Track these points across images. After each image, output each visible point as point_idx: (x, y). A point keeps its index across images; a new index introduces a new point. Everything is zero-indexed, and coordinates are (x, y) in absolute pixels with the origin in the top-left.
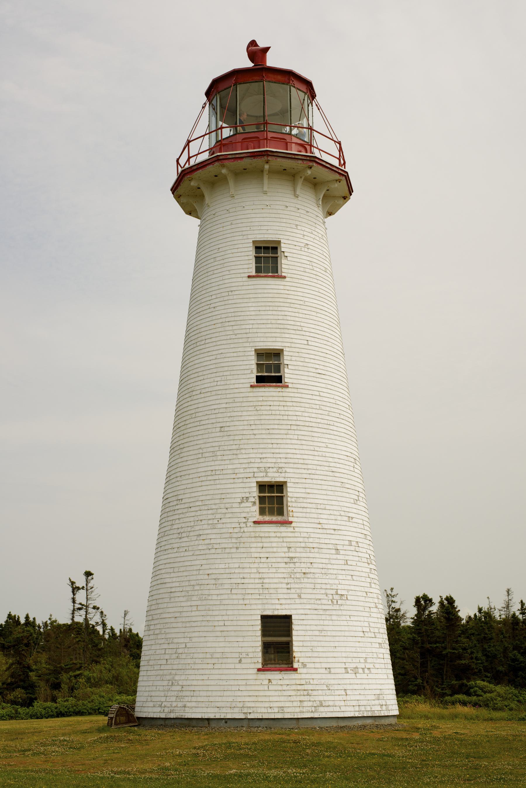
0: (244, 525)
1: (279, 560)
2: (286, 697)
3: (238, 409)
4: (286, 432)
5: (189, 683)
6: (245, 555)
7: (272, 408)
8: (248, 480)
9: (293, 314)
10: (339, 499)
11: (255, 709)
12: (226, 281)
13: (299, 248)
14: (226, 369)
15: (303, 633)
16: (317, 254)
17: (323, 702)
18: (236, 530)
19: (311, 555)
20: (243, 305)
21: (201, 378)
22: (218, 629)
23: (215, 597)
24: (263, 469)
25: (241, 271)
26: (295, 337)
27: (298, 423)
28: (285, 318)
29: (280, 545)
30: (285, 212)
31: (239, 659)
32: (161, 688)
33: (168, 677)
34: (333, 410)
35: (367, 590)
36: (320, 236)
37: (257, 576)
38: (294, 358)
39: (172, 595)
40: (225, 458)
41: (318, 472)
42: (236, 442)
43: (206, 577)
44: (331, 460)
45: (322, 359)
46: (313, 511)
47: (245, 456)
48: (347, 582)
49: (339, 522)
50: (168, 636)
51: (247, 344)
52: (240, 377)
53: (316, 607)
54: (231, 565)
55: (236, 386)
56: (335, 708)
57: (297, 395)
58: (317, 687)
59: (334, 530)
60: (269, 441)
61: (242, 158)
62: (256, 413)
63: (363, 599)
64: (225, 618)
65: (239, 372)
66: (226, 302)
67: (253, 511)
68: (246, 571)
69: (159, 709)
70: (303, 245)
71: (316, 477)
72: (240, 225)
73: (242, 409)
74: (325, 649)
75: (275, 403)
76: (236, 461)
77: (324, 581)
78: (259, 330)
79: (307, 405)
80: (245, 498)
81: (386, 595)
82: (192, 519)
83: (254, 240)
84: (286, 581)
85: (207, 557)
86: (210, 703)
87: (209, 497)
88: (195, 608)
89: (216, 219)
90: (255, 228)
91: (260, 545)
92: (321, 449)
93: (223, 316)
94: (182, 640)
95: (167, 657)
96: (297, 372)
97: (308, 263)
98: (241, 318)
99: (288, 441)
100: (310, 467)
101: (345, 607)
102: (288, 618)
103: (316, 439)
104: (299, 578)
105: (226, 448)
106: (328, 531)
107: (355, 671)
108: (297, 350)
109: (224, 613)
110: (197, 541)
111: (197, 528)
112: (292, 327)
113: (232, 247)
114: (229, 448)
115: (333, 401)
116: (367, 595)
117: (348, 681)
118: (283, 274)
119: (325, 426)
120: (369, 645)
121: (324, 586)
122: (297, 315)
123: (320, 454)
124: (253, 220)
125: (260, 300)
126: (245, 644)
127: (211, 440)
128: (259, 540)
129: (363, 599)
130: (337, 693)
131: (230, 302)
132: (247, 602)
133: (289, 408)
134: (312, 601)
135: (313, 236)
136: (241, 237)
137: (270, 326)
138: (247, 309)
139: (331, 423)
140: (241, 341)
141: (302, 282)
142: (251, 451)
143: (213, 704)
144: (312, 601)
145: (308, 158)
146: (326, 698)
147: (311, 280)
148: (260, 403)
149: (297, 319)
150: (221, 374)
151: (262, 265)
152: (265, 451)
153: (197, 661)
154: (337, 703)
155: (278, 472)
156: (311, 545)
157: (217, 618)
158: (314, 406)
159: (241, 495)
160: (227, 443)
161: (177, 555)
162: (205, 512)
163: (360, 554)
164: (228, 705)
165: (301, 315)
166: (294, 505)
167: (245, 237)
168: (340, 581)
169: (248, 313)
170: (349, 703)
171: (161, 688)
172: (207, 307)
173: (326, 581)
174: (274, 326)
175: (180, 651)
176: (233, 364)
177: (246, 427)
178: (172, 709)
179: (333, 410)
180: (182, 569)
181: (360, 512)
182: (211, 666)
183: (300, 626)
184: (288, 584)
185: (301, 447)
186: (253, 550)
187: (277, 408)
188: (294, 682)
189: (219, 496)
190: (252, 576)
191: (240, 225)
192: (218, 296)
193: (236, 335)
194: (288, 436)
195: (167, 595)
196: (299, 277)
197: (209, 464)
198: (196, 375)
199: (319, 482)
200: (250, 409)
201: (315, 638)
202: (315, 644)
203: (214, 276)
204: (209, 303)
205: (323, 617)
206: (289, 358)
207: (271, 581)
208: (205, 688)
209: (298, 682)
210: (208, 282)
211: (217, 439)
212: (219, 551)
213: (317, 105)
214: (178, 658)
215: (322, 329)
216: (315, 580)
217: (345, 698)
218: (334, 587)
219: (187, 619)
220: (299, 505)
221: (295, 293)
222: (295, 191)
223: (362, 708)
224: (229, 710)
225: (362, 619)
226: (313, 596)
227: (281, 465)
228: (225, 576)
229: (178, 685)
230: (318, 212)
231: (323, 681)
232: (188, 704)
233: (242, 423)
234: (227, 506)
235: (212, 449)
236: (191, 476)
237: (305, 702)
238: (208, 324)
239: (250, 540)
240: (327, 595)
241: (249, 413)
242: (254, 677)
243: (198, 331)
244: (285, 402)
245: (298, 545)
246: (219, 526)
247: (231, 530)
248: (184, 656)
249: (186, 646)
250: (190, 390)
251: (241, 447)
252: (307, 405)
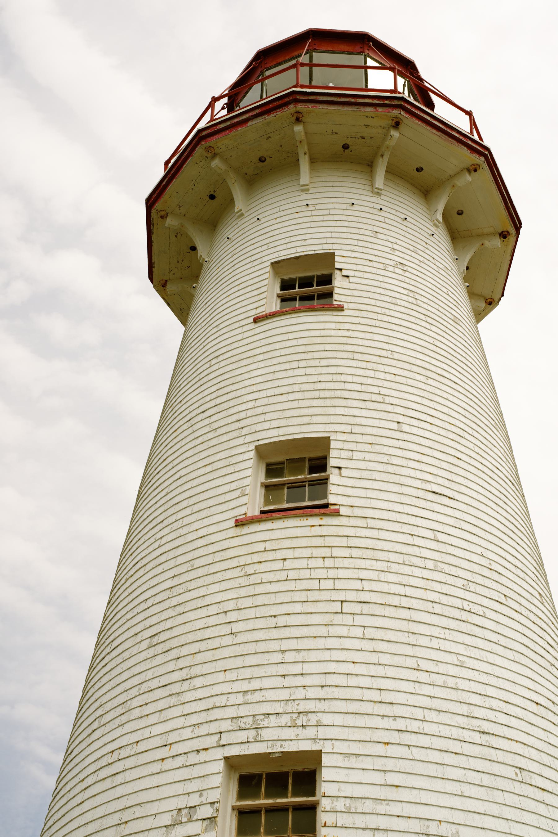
4: (327, 619)
8: (203, 757)
24: (250, 720)
26: (364, 413)
41: (428, 728)
57: (364, 532)
62: (243, 581)
78: (267, 409)
79: (393, 557)
122: (372, 373)
133: (338, 563)
145: (387, 102)
159: (173, 804)
185: (373, 658)
187: (304, 563)
194: (333, 631)
222: (372, 185)
227: (303, 706)
252: (393, 557)
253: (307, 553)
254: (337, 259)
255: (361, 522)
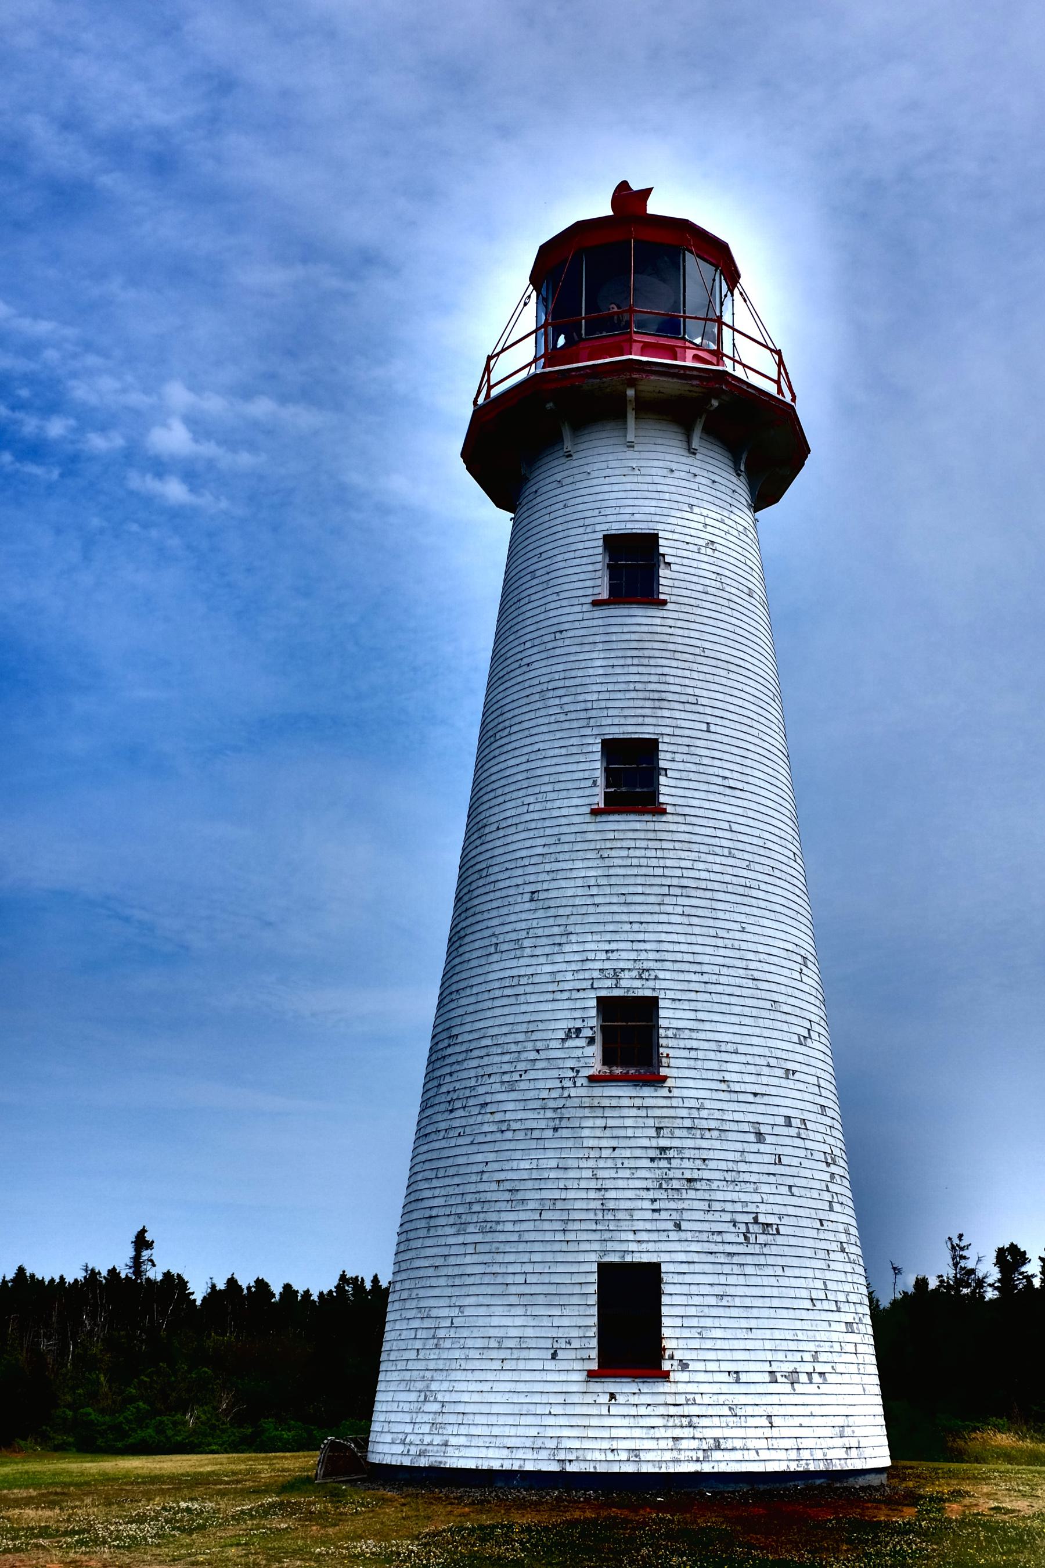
0: (570, 1084)
1: (638, 1153)
2: (645, 1430)
3: (567, 856)
4: (658, 899)
5: (455, 1397)
6: (570, 1143)
7: (632, 853)
8: (581, 994)
9: (680, 672)
10: (767, 1033)
11: (580, 1453)
12: (552, 614)
13: (695, 548)
14: (546, 779)
15: (682, 1300)
16: (732, 560)
17: (721, 1441)
18: (555, 1094)
19: (704, 1144)
20: (581, 657)
21: (501, 800)
22: (513, 1289)
23: (509, 1227)
24: (612, 972)
25: (581, 593)
27: (685, 882)
28: (663, 679)
29: (640, 1122)
30: (669, 481)
31: (552, 1351)
32: (406, 1407)
33: (420, 1386)
34: (757, 859)
35: (822, 1215)
36: (741, 529)
37: (593, 1184)
38: (678, 757)
39: (433, 1222)
40: (538, 951)
41: (723, 980)
42: (560, 921)
43: (494, 1186)
44: (750, 956)
45: (739, 760)
46: (712, 1055)
47: (576, 948)
48: (778, 1199)
49: (764, 1080)
50: (423, 1303)
51: (588, 731)
52: (572, 793)
53: (713, 1248)
54: (543, 1164)
55: (564, 812)
56: (745, 1452)
58: (710, 1411)
59: (755, 1094)
60: (625, 918)
62: (600, 863)
63: (813, 1233)
64: (528, 1268)
65: (569, 785)
66: (551, 653)
67: (591, 1058)
68: (571, 1174)
69: (399, 1449)
70: (703, 543)
71: (719, 989)
72: (581, 507)
73: (574, 856)
74: (728, 1334)
75: (639, 844)
76: (559, 958)
77: (729, 1196)
78: (610, 704)
79: (703, 848)
80: (573, 1031)
81: (950, 1246)
82: (473, 1073)
83: (606, 533)
84: (651, 1195)
85: (498, 1146)
86: (493, 1439)
87: (505, 1030)
88: (470, 1249)
89: (539, 499)
90: (608, 511)
91: (600, 1123)
92: (731, 935)
93: (544, 679)
94: (445, 1312)
95: (418, 1344)
96: (685, 784)
97: (714, 576)
98: (578, 681)
99: (663, 918)
100: (705, 968)
101: (774, 1250)
102: (654, 1269)
103: (720, 915)
104: (678, 1189)
105: (540, 932)
106: (742, 1097)
107: (792, 1377)
108: (686, 741)
109: (525, 1258)
110: (480, 1117)
111: (481, 1090)
112: (676, 697)
113: (563, 550)
114: (547, 931)
115: (760, 842)
116: (822, 1225)
117: (775, 1399)
118: (662, 597)
119: (741, 890)
120: (825, 1326)
121: (729, 1207)
122: (687, 673)
123: (729, 943)
124: (606, 496)
125: (614, 646)
126: (565, 1321)
127: (513, 918)
128: (599, 1113)
129: (813, 1233)
130: (751, 1422)
131: (558, 652)
132: (571, 1236)
133: (666, 854)
134: (704, 1237)
135: (726, 528)
136: (581, 530)
137: (633, 695)
138: (589, 664)
139: (755, 884)
140: (575, 724)
141: (699, 611)
142: (589, 937)
143: (499, 1442)
144: (704, 1237)
146: (728, 1433)
147: (719, 608)
148: (609, 845)
149: (687, 682)
150: (537, 790)
152: (617, 937)
153: (473, 1354)
154: (750, 1444)
155: (641, 978)
156: (704, 1124)
157: (511, 1269)
158: (718, 850)
159: (564, 1025)
160: (542, 923)
161: (444, 1143)
162: (497, 1059)
163: (809, 1144)
164: (528, 1443)
165: (695, 675)
166: (672, 1043)
167: (589, 529)
168: (764, 1196)
169: (591, 672)
170: (775, 1443)
171: (406, 1407)
172: (517, 665)
173: (734, 1196)
174: (641, 695)
175: (441, 1333)
176: (558, 769)
177: (580, 891)
178: (423, 1448)
179: (757, 859)
180: (452, 1171)
181: (813, 1062)
182: (497, 1365)
183: (678, 1286)
185: (689, 930)
186: (586, 1133)
187: (642, 853)
188: (661, 1399)
189: (524, 1027)
190: (584, 1184)
191: (581, 507)
192: (536, 642)
193: (566, 713)
194: (664, 908)
195: (423, 1224)
196: (693, 602)
197: (508, 964)
198: (492, 795)
199: (726, 999)
200: (589, 855)
201: (707, 1311)
202: (708, 1322)
203: (530, 606)
204: (519, 656)
205: (727, 1269)
206: (669, 756)
207: (620, 1194)
208: (485, 1409)
209: (670, 1399)
210: (520, 619)
211: (524, 916)
212: (520, 1135)
213: (741, 294)
214: (437, 1347)
215: (740, 702)
216: (711, 1193)
217: (768, 1432)
218: (751, 1208)
219: (457, 1271)
220: (682, 1043)
221: (686, 633)
222: (689, 442)
223: (806, 1454)
224: (529, 1455)
225: (810, 1273)
226: (706, 1227)
228: (529, 1185)
229: (436, 1401)
230: (743, 495)
231: (721, 1399)
232: (453, 1441)
233: (572, 883)
234: (540, 1045)
235: (514, 936)
236: (475, 990)
237: (683, 1441)
238: (516, 696)
239: (580, 1113)
240: (735, 1224)
241: (587, 864)
242: (582, 1388)
243: (499, 712)
244: (658, 842)
245: (678, 1123)
246: (523, 1085)
247: (544, 1094)
248: (448, 1344)
249: (452, 1323)
250: (480, 825)
251: (570, 929)
252: (703, 848)
253: (643, 844)
254: (661, 542)
255: (680, 819)
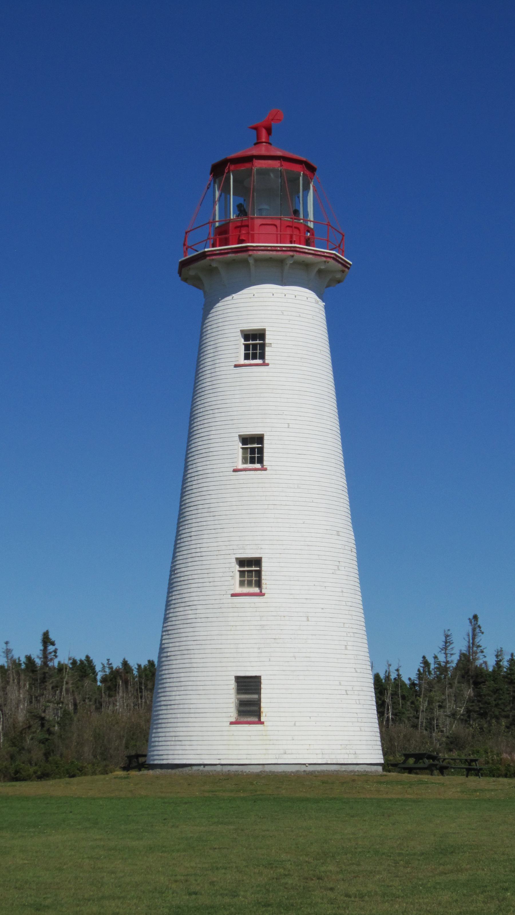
57: (275, 476)
61: (228, 253)
151: (251, 352)
184: (259, 648)
223: (326, 756)
